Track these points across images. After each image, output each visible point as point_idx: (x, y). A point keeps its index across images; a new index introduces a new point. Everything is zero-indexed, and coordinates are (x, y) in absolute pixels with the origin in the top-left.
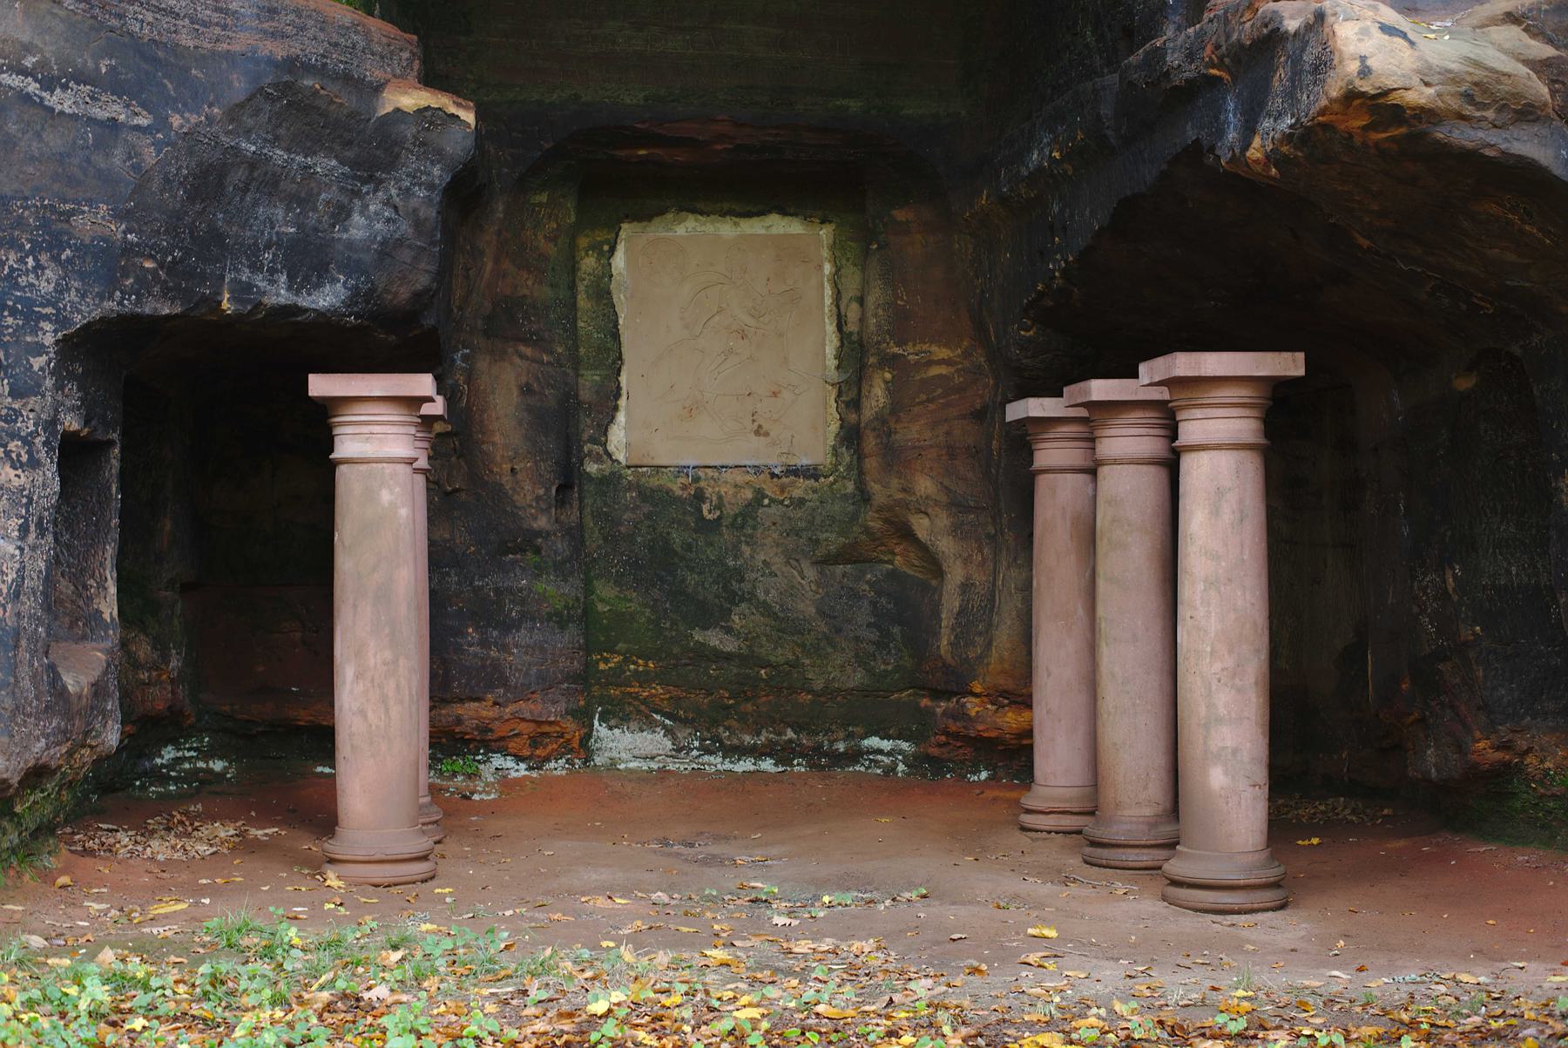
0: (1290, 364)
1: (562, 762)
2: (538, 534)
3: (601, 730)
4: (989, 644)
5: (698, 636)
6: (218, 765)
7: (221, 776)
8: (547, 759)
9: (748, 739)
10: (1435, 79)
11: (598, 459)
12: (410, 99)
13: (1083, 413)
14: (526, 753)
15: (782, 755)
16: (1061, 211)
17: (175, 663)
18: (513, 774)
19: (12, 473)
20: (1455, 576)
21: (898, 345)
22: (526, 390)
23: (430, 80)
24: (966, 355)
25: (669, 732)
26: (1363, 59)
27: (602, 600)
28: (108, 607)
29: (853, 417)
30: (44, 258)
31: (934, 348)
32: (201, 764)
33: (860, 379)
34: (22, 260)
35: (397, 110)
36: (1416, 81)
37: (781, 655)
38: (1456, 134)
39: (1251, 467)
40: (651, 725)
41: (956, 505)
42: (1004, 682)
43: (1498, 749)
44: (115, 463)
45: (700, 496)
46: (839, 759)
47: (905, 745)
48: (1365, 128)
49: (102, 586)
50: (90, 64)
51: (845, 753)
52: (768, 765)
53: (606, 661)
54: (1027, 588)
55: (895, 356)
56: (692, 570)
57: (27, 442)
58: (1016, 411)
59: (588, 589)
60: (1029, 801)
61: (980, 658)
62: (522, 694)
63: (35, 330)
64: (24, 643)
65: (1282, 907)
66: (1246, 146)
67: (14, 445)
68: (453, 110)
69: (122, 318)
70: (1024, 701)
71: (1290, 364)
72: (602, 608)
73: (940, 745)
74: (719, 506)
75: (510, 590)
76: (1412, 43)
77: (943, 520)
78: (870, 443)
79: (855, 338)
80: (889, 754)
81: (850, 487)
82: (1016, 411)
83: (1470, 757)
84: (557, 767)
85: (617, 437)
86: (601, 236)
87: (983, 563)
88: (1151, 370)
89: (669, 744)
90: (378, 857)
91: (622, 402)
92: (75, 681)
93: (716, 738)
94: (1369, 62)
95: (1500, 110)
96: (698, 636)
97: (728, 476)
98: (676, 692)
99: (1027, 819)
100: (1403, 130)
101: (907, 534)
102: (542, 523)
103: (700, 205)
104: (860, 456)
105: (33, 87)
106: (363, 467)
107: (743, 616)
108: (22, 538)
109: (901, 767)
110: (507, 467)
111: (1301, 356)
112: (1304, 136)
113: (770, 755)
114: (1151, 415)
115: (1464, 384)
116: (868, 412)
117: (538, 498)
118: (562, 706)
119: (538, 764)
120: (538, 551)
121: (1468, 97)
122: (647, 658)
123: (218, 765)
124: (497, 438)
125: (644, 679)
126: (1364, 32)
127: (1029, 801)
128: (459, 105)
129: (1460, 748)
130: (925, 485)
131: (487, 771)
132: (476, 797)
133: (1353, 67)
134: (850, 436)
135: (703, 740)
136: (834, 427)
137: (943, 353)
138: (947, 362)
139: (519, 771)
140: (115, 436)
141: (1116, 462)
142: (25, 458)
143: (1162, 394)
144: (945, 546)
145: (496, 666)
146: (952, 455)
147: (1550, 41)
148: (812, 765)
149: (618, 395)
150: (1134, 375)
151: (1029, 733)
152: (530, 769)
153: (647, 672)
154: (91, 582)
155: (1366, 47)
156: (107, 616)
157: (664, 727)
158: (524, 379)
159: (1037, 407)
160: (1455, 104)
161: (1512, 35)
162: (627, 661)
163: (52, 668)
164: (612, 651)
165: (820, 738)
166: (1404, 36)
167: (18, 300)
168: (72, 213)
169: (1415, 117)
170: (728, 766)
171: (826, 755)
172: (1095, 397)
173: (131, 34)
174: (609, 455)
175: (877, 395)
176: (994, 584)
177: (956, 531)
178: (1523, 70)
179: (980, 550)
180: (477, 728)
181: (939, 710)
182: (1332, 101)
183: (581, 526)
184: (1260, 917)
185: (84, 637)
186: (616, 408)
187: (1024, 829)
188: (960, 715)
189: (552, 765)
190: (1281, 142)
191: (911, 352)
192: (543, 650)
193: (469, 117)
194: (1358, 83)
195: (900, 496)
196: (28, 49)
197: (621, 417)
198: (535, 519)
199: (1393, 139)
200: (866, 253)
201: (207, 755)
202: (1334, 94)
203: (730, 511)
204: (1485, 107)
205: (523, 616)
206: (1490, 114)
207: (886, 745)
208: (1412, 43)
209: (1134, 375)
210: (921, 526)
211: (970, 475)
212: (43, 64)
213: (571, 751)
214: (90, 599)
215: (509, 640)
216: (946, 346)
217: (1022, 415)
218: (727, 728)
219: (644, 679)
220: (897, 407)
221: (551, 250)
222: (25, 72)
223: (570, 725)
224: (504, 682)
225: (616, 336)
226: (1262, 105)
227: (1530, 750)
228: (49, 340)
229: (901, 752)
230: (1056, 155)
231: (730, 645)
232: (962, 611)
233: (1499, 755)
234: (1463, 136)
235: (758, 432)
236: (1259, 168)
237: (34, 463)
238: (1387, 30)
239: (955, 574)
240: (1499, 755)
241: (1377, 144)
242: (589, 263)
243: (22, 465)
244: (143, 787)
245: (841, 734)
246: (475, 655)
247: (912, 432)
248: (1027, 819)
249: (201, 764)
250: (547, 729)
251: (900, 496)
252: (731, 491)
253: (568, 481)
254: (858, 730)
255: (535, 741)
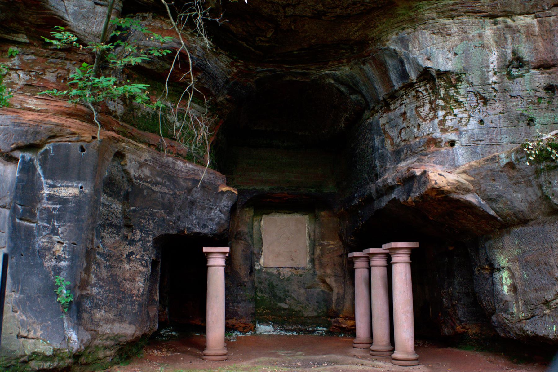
0: (414, 245)
1: (250, 333)
2: (245, 282)
3: (258, 325)
4: (344, 306)
5: (279, 304)
6: (174, 333)
7: (175, 336)
8: (247, 332)
9: (290, 327)
10: (450, 184)
11: (258, 266)
12: (225, 189)
13: (367, 255)
14: (242, 331)
15: (298, 331)
16: (361, 212)
17: (167, 310)
18: (239, 336)
19: (143, 268)
20: (451, 290)
21: (323, 241)
22: (243, 251)
23: (228, 185)
24: (337, 243)
25: (273, 326)
26: (435, 181)
27: (258, 296)
28: (157, 298)
29: (313, 257)
30: (151, 222)
31: (330, 242)
32: (170, 333)
33: (314, 248)
34: (146, 222)
35: (222, 191)
36: (446, 185)
37: (298, 309)
38: (455, 196)
39: (408, 267)
40: (268, 324)
41: (336, 276)
42: (348, 315)
43: (462, 328)
44: (160, 266)
45: (279, 273)
46: (310, 332)
47: (325, 329)
48: (436, 195)
49: (156, 293)
50: (161, 181)
51: (312, 331)
52: (295, 333)
53: (259, 310)
54: (354, 293)
55: (322, 243)
56: (278, 290)
57: (146, 261)
58: (350, 255)
59: (256, 294)
60: (355, 341)
61: (342, 309)
62: (241, 317)
63: (148, 237)
64: (144, 306)
65: (418, 365)
66: (407, 199)
67: (143, 262)
68: (233, 191)
69: (165, 235)
70: (354, 319)
71: (414, 245)
72: (258, 298)
73: (333, 329)
74: (284, 276)
75: (239, 294)
76: (445, 177)
77: (333, 279)
78: (317, 262)
79: (313, 239)
80: (321, 331)
81: (312, 272)
82: (350, 255)
83: (456, 330)
84: (249, 334)
85: (262, 261)
86: (259, 218)
87: (342, 288)
88: (386, 246)
89: (273, 329)
90: (216, 354)
91: (263, 253)
92: (152, 314)
93: (283, 327)
94: (437, 181)
95: (463, 191)
96: (279, 304)
97: (280, 269)
98: (275, 317)
99: (355, 345)
100: (444, 195)
101: (324, 282)
102: (246, 279)
103: (279, 211)
104: (314, 265)
105: (150, 185)
106: (214, 267)
107: (289, 300)
108: (144, 282)
109: (324, 334)
110: (239, 267)
111: (418, 243)
112: (422, 197)
113: (295, 331)
114: (383, 256)
115: (451, 248)
116: (316, 256)
117: (245, 274)
118: (250, 320)
119: (244, 333)
120: (245, 286)
121: (457, 188)
122: (268, 310)
123: (174, 333)
124: (237, 261)
125: (268, 314)
126: (435, 175)
127: (355, 341)
128: (234, 190)
129: (453, 328)
130: (329, 271)
131: (234, 334)
132: (231, 341)
133: (433, 182)
134: (312, 261)
135: (280, 328)
136: (308, 259)
137: (332, 243)
138: (333, 245)
139: (240, 335)
140: (160, 260)
141: (376, 266)
142: (145, 265)
143: (387, 251)
144: (333, 285)
145: (236, 312)
146: (335, 265)
147: (473, 177)
148: (305, 334)
149: (262, 252)
150: (381, 247)
151: (354, 325)
152: (243, 334)
153: (268, 313)
154: (154, 292)
155: (435, 179)
156: (157, 300)
157: (272, 325)
158: (242, 248)
159: (356, 254)
160: (454, 190)
161: (465, 176)
162: (264, 310)
163: (148, 311)
164: (260, 308)
165: (306, 327)
166: (443, 176)
167: (145, 231)
168: (156, 212)
169: (447, 193)
170: (286, 334)
171: (307, 331)
172: (371, 252)
173: (169, 174)
174: (260, 265)
175: (318, 251)
176: (344, 293)
177: (336, 281)
178: (468, 183)
179: (341, 285)
180: (232, 325)
181: (332, 321)
182: (428, 189)
183: (254, 280)
184: (414, 367)
185: (151, 305)
186: (262, 255)
187: (354, 347)
188: (337, 322)
189: (248, 333)
190: (416, 198)
191: (325, 243)
192: (246, 308)
193: (236, 193)
194: (434, 185)
195: (323, 274)
196: (149, 177)
197: (262, 256)
198: (244, 278)
199: (441, 197)
200: (315, 221)
201: (171, 331)
202: (429, 188)
203: (286, 277)
204: (460, 190)
205: (242, 300)
206: (461, 192)
207: (321, 329)
208: (445, 177)
209: (381, 247)
210: (328, 280)
211: (83, 303)
212: (152, 180)
213: (252, 330)
214: (153, 296)
215: (239, 305)
216: (333, 241)
217: (352, 256)
218: (286, 325)
219: (268, 314)
220: (323, 254)
221: (248, 220)
222: (148, 182)
223: (252, 324)
224: (238, 315)
225: (261, 239)
226: (411, 190)
227: (469, 328)
228: (151, 239)
229: (324, 330)
230: (360, 200)
231: (286, 306)
232: (337, 299)
233: (462, 330)
234: (455, 196)
235: (292, 260)
236: (410, 203)
237: (147, 266)
238: (440, 175)
239: (336, 291)
240: (462, 330)
241: (438, 198)
242: (256, 223)
243: (145, 266)
244: (158, 338)
245: (311, 326)
246: (232, 309)
247: (325, 260)
248: (355, 345)
249: (170, 333)
250: (246, 325)
251: (323, 274)
252: (286, 273)
253: (252, 270)
254: (315, 326)
255: (244, 328)
